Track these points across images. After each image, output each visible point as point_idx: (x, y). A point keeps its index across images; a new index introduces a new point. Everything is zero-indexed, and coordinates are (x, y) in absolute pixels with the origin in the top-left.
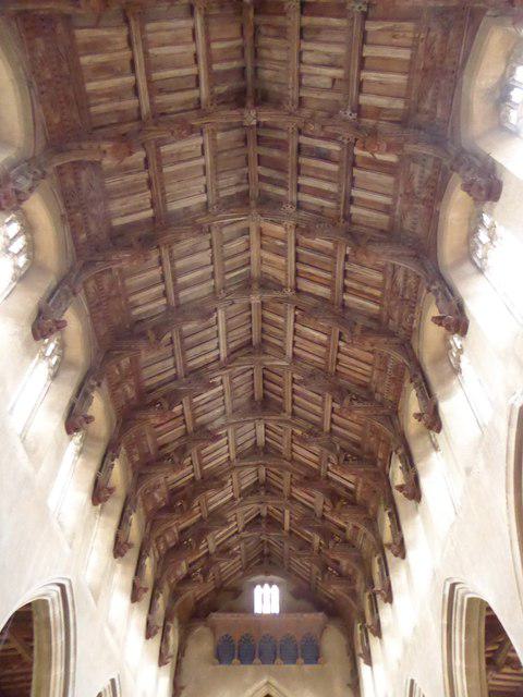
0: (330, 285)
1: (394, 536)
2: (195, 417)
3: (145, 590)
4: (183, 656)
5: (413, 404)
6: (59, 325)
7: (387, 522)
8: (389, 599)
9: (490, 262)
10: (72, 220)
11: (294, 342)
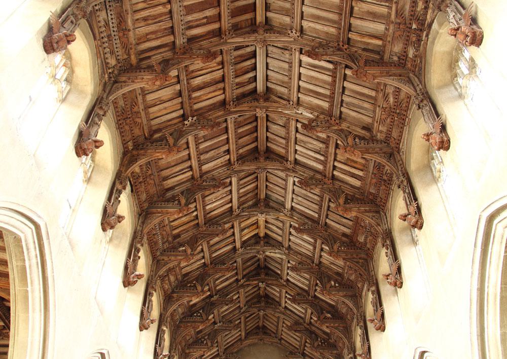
0: (324, 163)
1: (376, 311)
2: (215, 287)
3: (152, 321)
5: (399, 205)
6: (69, 38)
7: (359, 331)
8: (382, 328)
9: (443, 175)
10: (139, 199)
11: (293, 198)
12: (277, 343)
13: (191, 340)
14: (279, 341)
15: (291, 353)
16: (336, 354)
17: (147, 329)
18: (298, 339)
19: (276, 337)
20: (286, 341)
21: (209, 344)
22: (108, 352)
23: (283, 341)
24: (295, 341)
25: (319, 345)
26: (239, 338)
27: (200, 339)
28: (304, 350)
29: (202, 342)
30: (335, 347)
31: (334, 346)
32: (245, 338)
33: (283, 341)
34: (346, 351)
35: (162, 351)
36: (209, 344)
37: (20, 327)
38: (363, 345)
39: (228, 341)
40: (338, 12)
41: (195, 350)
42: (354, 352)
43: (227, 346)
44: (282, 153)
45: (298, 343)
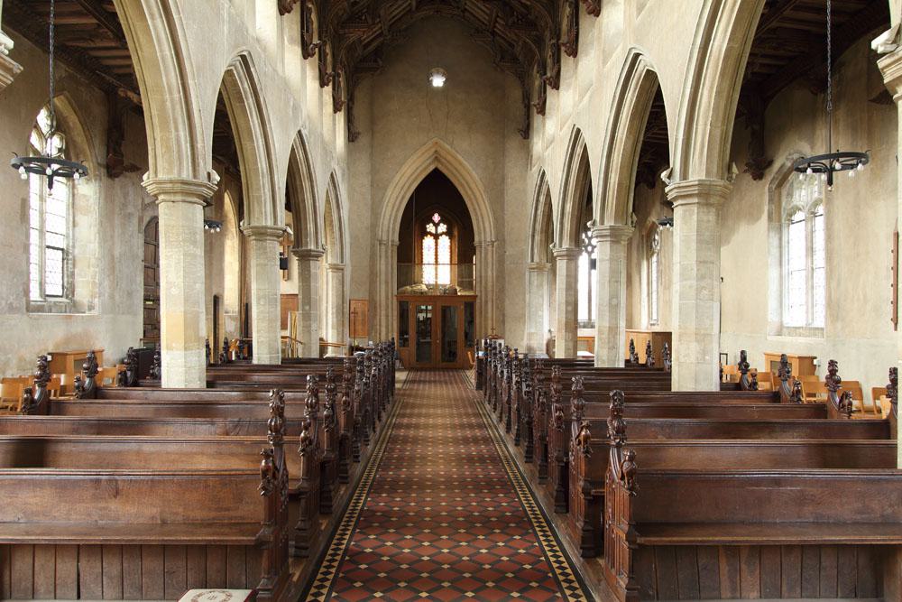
4: (353, 103)
12: (459, 16)
13: (345, 16)
14: (462, 14)
15: (477, 31)
16: (536, 36)
17: (289, 12)
18: (488, 12)
19: (458, 8)
20: (472, 14)
21: (370, 21)
22: (250, 53)
23: (467, 14)
24: (483, 14)
25: (514, 23)
26: (408, 9)
27: (357, 14)
28: (495, 27)
29: (360, 18)
30: (536, 25)
31: (532, 25)
32: (417, 7)
33: (467, 14)
34: (547, 34)
35: (312, 39)
36: (370, 21)
37: (141, 40)
38: (569, 31)
39: (394, 14)
40: (546, 298)
41: (351, 30)
42: (559, 39)
43: (393, 21)
44: (529, 328)
45: (487, 18)
